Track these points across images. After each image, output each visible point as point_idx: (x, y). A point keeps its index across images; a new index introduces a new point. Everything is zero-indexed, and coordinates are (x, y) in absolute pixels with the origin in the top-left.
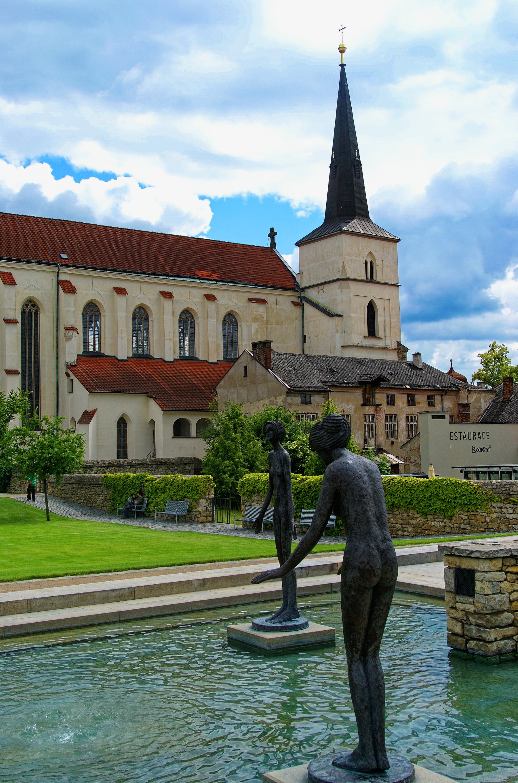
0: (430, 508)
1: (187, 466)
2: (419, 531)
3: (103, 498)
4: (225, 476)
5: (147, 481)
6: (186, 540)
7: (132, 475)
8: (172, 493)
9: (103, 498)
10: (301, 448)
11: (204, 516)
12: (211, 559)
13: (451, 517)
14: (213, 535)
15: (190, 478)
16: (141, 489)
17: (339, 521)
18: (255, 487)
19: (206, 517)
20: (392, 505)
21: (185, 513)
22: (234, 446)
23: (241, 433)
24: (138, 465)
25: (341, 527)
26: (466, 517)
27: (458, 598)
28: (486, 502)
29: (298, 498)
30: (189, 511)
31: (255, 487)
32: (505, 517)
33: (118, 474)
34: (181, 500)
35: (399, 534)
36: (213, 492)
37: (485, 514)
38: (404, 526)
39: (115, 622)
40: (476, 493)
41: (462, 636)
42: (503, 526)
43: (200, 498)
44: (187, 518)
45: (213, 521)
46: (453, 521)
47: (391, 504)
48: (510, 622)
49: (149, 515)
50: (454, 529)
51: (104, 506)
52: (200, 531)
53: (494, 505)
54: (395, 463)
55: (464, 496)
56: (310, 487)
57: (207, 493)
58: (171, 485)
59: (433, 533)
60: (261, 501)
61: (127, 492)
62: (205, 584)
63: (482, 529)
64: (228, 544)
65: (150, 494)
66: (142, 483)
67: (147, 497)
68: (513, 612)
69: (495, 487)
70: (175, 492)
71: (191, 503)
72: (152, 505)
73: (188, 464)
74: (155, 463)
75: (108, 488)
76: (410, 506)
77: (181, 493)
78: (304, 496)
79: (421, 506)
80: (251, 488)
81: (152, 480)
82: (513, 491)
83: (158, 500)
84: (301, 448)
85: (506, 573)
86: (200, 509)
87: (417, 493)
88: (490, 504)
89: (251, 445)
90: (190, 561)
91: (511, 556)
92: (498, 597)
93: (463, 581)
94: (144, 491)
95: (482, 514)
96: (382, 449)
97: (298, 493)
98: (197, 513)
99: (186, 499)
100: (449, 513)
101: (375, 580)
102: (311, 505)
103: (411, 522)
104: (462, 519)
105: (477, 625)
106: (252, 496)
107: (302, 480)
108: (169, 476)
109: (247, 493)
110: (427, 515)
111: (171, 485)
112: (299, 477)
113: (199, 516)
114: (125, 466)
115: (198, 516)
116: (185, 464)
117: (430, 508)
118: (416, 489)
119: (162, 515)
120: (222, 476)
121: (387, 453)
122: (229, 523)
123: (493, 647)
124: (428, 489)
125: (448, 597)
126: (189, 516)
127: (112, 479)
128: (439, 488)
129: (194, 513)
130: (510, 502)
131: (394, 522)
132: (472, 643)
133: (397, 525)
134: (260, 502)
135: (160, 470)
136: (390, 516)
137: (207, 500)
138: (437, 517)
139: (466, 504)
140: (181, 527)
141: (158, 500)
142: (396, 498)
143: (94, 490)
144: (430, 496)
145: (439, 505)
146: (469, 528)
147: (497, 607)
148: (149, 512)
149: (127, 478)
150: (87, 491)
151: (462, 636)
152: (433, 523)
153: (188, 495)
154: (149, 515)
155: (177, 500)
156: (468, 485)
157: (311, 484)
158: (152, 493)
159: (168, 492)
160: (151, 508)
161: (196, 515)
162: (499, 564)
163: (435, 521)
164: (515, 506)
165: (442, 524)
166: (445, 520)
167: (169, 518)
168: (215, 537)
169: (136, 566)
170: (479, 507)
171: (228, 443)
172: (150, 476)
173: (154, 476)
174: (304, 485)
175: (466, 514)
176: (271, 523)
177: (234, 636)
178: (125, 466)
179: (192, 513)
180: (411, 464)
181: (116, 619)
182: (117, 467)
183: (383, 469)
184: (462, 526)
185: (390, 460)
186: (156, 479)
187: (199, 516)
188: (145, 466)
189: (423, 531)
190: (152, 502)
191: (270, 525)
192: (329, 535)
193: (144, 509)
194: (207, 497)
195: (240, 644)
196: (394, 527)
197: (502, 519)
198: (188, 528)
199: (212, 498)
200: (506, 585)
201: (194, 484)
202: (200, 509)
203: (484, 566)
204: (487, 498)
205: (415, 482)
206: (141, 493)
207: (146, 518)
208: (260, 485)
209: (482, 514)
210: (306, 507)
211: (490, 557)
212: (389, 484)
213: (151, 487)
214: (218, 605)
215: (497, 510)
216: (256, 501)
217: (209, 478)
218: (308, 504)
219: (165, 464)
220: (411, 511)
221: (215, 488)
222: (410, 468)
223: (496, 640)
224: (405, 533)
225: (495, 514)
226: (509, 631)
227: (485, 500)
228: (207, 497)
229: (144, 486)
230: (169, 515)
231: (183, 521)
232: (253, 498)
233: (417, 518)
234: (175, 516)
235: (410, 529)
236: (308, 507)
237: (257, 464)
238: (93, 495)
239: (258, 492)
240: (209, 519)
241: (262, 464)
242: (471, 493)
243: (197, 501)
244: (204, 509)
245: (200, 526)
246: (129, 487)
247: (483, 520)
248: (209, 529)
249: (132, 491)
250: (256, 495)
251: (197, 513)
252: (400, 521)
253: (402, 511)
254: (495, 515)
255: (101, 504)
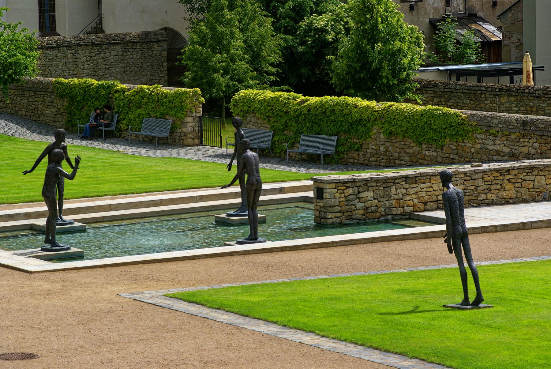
0: (424, 138)
1: (156, 46)
2: (414, 160)
3: (54, 110)
4: (215, 75)
5: (116, 92)
6: (173, 167)
7: (96, 82)
8: (149, 108)
9: (54, 110)
10: (332, 25)
11: (191, 138)
12: (203, 185)
13: (442, 146)
14: (202, 162)
15: (173, 92)
16: (109, 102)
17: (339, 148)
18: (250, 107)
19: (193, 139)
20: (390, 133)
21: (166, 134)
22: (228, 31)
23: (242, 7)
24: (79, 45)
25: (341, 155)
26: (455, 148)
27: (318, 201)
28: (471, 133)
29: (297, 122)
30: (172, 132)
31: (250, 107)
32: (486, 149)
33: (76, 80)
34: (161, 118)
35: (397, 163)
36: (201, 109)
37: (471, 145)
38: (401, 155)
39: (156, 216)
40: (463, 123)
41: (319, 217)
42: (484, 157)
43: (186, 116)
44: (170, 140)
45: (201, 144)
46: (444, 151)
47: (389, 131)
48: (339, 210)
49: (120, 134)
50: (445, 159)
51: (56, 121)
52: (187, 157)
53: (478, 136)
54: (494, 39)
55: (452, 126)
56: (309, 110)
57: (194, 110)
58: (149, 99)
59: (426, 162)
60: (258, 123)
61: (89, 104)
62: (202, 198)
63: (468, 160)
64: (219, 173)
65: (121, 109)
66: (110, 93)
67: (117, 112)
68: (340, 207)
69: (479, 119)
70: (153, 108)
71: (174, 123)
72: (124, 122)
73: (158, 41)
74: (106, 41)
75: (62, 97)
76: (406, 135)
77: (161, 109)
78: (304, 120)
79: (415, 135)
80: (245, 108)
81: (123, 91)
82: (493, 123)
83: (131, 116)
84: (332, 25)
85: (338, 189)
86: (184, 130)
87: (412, 122)
88: (474, 135)
89: (254, 25)
90: (188, 187)
91: (340, 182)
92: (333, 200)
93: (320, 193)
94: (112, 103)
95: (468, 145)
96: (476, 15)
97: (297, 116)
98: (182, 135)
99: (167, 117)
100: (440, 143)
101: (254, 188)
102: (311, 130)
103: (408, 151)
104: (452, 149)
105: (324, 212)
106: (247, 117)
107: (303, 102)
108: (145, 87)
109: (242, 113)
110: (421, 144)
111: (149, 99)
112: (299, 98)
113: (185, 138)
114: (59, 47)
115: (183, 138)
116: (153, 42)
117: (424, 138)
118: (412, 117)
119: (137, 136)
120: (212, 76)
121: (485, 21)
122: (221, 147)
123: (330, 221)
124: (422, 118)
125: (314, 201)
126: (172, 137)
127: (67, 86)
128: (432, 117)
129: (178, 134)
130: (491, 134)
131: (392, 151)
132: (322, 220)
133: (395, 154)
134: (256, 124)
135: (113, 53)
136: (389, 144)
137: (194, 119)
138: (430, 146)
139: (455, 135)
140: (163, 153)
141: (131, 116)
142: (393, 126)
143: (41, 100)
144: (424, 126)
145: (431, 134)
146: (457, 158)
147: (333, 204)
148: (120, 131)
149: (89, 86)
150: (31, 99)
151: (319, 217)
152: (427, 153)
153: (170, 112)
154: (120, 134)
155: (156, 117)
156: (457, 116)
157: (311, 107)
158: (123, 108)
159: (145, 107)
160: (123, 126)
161: (180, 136)
162: (334, 185)
163: (428, 150)
164: (494, 138)
165: (434, 154)
166: (438, 150)
167: (146, 139)
168: (205, 165)
169: (151, 190)
170: (466, 138)
171: (220, 28)
172: (120, 86)
173: (125, 86)
174: (304, 107)
175: (455, 144)
176: (268, 149)
177: (217, 220)
178: (59, 47)
179: (175, 134)
180: (512, 45)
181: (156, 215)
182: (47, 48)
183: (467, 53)
184: (452, 156)
185: (488, 34)
186: (129, 90)
187: (185, 138)
188: (90, 47)
189: (418, 160)
190: (124, 119)
191: (267, 151)
192: (328, 163)
193: (113, 128)
194: (194, 115)
195: (220, 222)
196: (392, 156)
197: (484, 150)
198: (173, 153)
199: (200, 117)
200: (337, 195)
201: (178, 100)
202: (184, 130)
203: (327, 186)
204: (471, 130)
205: (411, 110)
206: (109, 107)
207: (117, 139)
208: (256, 105)
209: (468, 145)
210: (306, 132)
211: (329, 182)
212: (388, 111)
213: (123, 99)
214: (210, 209)
215: (480, 141)
216: (251, 123)
217: (196, 91)
218: (307, 128)
219: (120, 43)
220: (408, 139)
221: (203, 104)
222: (510, 51)
223: (331, 218)
224: (402, 162)
225: (479, 145)
226: (339, 215)
227: (471, 131)
228: (194, 115)
229: (112, 98)
230: (147, 136)
231: (164, 144)
232: (249, 118)
233: (412, 147)
234: (154, 137)
235: (407, 158)
236: (308, 132)
237: (264, 53)
238: (40, 106)
239: (253, 111)
240: (197, 141)
241: (272, 51)
242: (458, 123)
243: (181, 120)
244: (190, 129)
245: (185, 150)
246: (92, 98)
247: (468, 150)
248: (197, 154)
249: (97, 103)
250: (251, 116)
251: (182, 135)
252: (398, 150)
253: (400, 140)
254: (478, 146)
255: (52, 119)
